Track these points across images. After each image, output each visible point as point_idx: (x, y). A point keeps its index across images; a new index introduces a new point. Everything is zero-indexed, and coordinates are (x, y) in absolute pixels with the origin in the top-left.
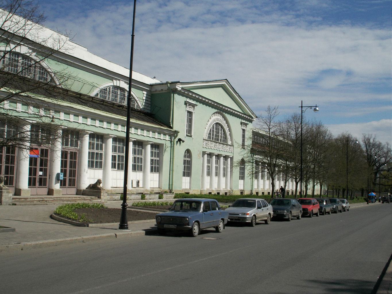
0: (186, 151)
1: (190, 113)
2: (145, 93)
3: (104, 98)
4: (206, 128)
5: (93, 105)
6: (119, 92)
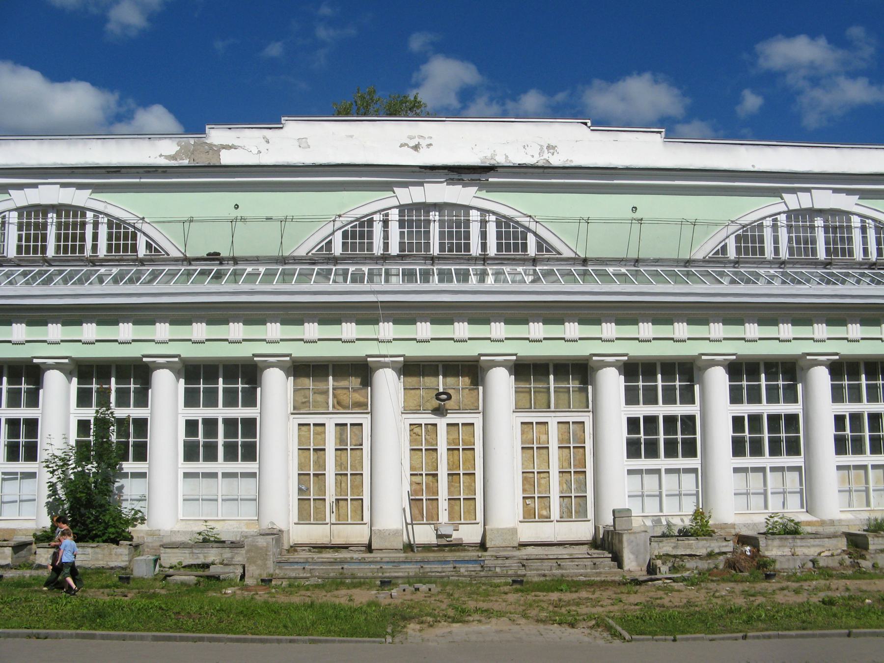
5: (345, 273)
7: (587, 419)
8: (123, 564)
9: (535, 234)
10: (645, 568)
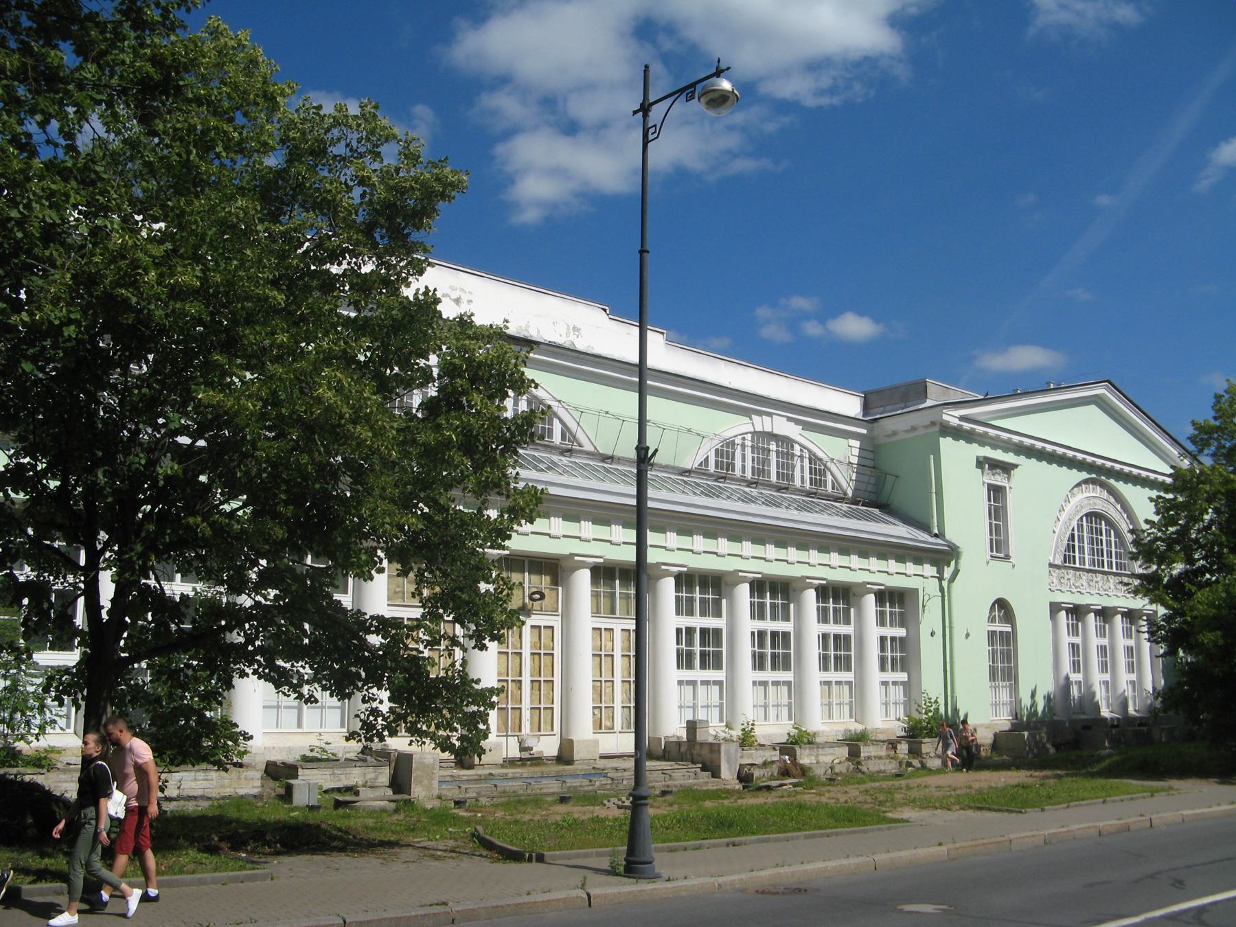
0: (993, 604)
1: (996, 492)
2: (856, 443)
3: (727, 470)
4: (1054, 532)
6: (773, 447)
7: (555, 622)
8: (255, 791)
9: (561, 421)
10: (735, 777)
